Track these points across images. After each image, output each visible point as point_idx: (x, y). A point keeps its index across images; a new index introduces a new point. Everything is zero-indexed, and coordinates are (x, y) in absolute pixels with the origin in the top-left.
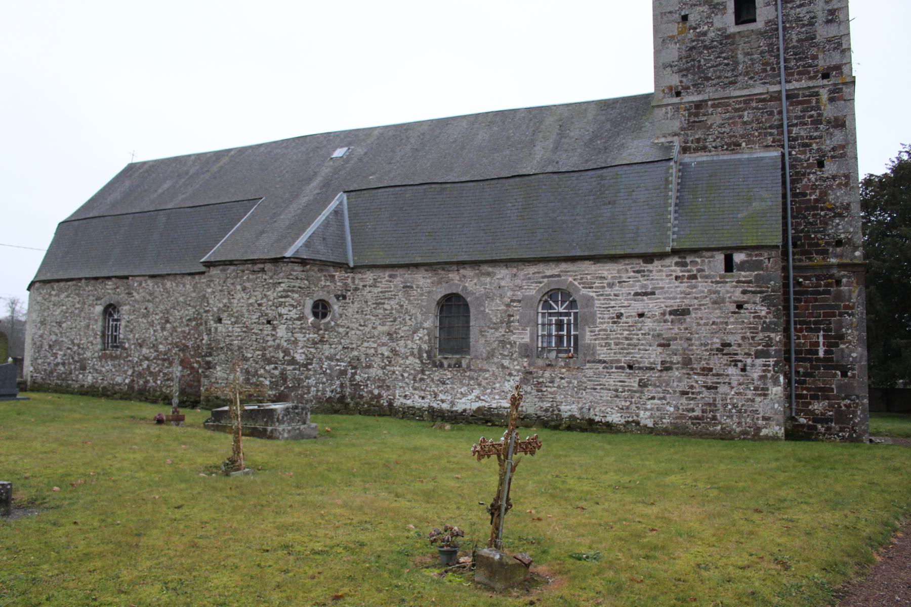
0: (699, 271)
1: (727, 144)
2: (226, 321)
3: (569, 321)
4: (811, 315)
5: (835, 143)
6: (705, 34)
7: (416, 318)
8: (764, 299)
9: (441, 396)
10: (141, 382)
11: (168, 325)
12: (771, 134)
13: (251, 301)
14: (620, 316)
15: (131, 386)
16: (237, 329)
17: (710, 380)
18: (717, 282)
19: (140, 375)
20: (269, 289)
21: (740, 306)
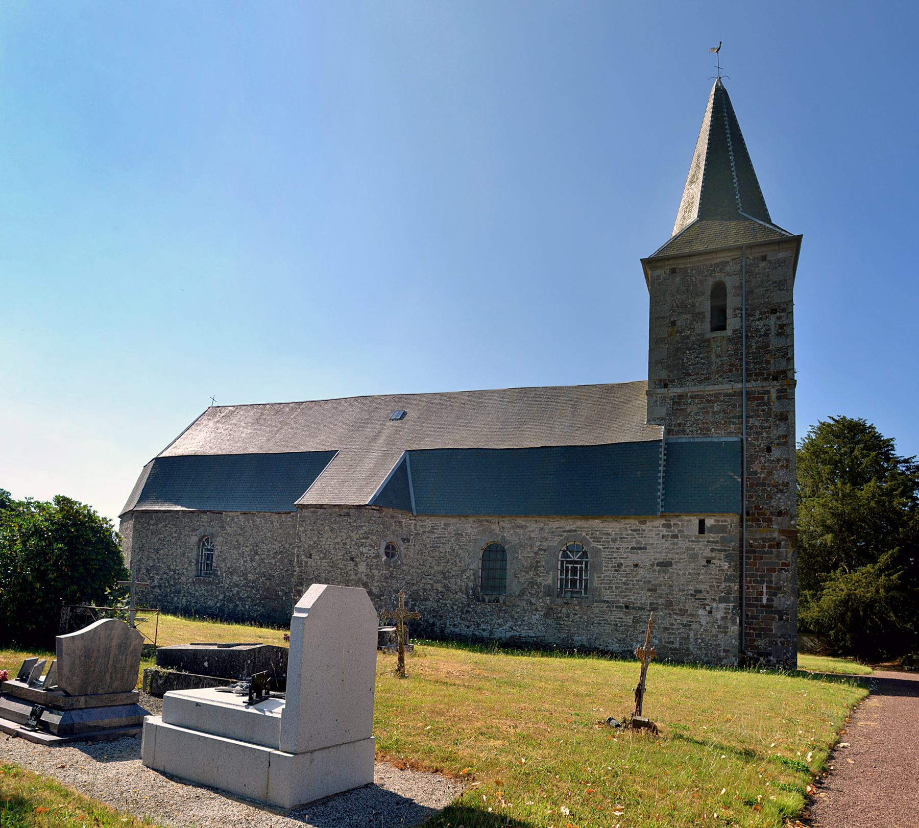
0: (679, 531)
1: (700, 429)
2: (316, 557)
3: (581, 568)
4: (757, 570)
5: (780, 433)
6: (688, 337)
7: (464, 561)
8: (726, 556)
9: (483, 626)
10: (231, 606)
11: (257, 557)
12: (734, 423)
13: (337, 540)
14: (620, 565)
15: (221, 610)
16: (325, 563)
17: (685, 620)
18: (693, 541)
19: (230, 600)
20: (352, 531)
21: (709, 562)
